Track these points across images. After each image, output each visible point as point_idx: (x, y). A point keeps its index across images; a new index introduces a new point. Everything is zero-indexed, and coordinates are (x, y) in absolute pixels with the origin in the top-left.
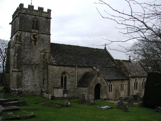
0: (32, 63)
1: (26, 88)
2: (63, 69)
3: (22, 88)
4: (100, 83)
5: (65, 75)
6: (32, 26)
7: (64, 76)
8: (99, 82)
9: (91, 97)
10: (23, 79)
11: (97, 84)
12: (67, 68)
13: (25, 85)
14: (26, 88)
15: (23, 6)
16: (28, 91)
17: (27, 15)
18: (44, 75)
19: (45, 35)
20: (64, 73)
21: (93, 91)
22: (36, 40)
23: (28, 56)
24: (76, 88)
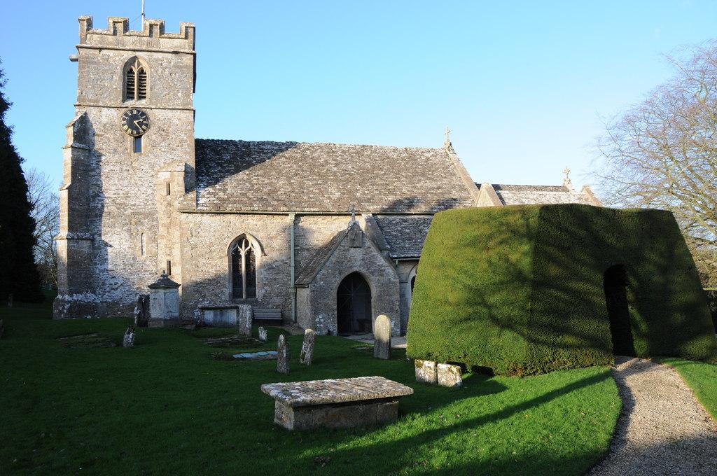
0: (129, 212)
1: (109, 292)
2: (238, 225)
3: (94, 292)
4: (363, 271)
5: (246, 246)
6: (128, 89)
7: (243, 252)
8: (356, 269)
9: (320, 323)
10: (96, 264)
11: (347, 274)
12: (252, 221)
13: (104, 284)
14: (109, 292)
15: (5, 110)
16: (115, 303)
17: (104, 52)
18: (171, 249)
19: (170, 114)
20: (241, 240)
21: (332, 301)
22: (138, 133)
23: (113, 188)
24: (292, 290)
